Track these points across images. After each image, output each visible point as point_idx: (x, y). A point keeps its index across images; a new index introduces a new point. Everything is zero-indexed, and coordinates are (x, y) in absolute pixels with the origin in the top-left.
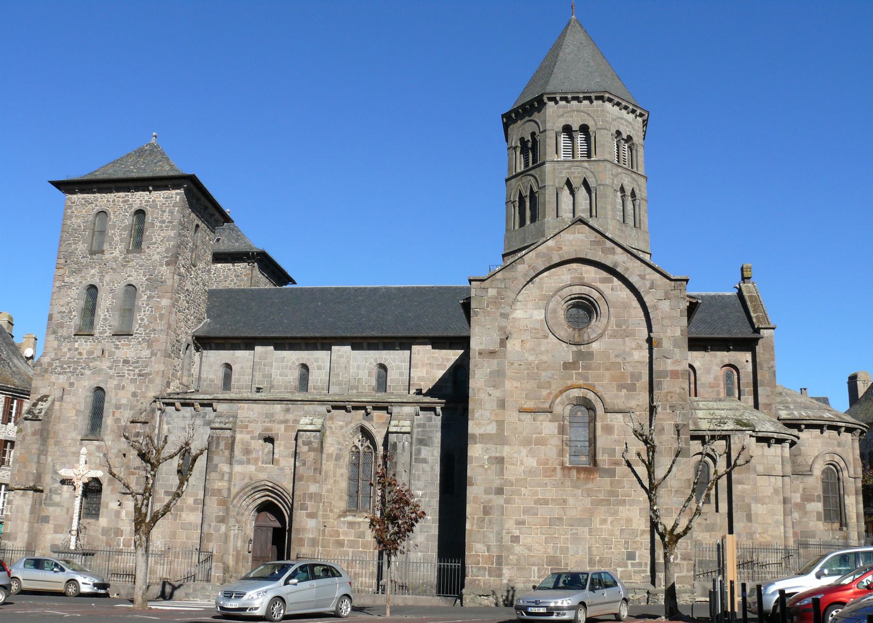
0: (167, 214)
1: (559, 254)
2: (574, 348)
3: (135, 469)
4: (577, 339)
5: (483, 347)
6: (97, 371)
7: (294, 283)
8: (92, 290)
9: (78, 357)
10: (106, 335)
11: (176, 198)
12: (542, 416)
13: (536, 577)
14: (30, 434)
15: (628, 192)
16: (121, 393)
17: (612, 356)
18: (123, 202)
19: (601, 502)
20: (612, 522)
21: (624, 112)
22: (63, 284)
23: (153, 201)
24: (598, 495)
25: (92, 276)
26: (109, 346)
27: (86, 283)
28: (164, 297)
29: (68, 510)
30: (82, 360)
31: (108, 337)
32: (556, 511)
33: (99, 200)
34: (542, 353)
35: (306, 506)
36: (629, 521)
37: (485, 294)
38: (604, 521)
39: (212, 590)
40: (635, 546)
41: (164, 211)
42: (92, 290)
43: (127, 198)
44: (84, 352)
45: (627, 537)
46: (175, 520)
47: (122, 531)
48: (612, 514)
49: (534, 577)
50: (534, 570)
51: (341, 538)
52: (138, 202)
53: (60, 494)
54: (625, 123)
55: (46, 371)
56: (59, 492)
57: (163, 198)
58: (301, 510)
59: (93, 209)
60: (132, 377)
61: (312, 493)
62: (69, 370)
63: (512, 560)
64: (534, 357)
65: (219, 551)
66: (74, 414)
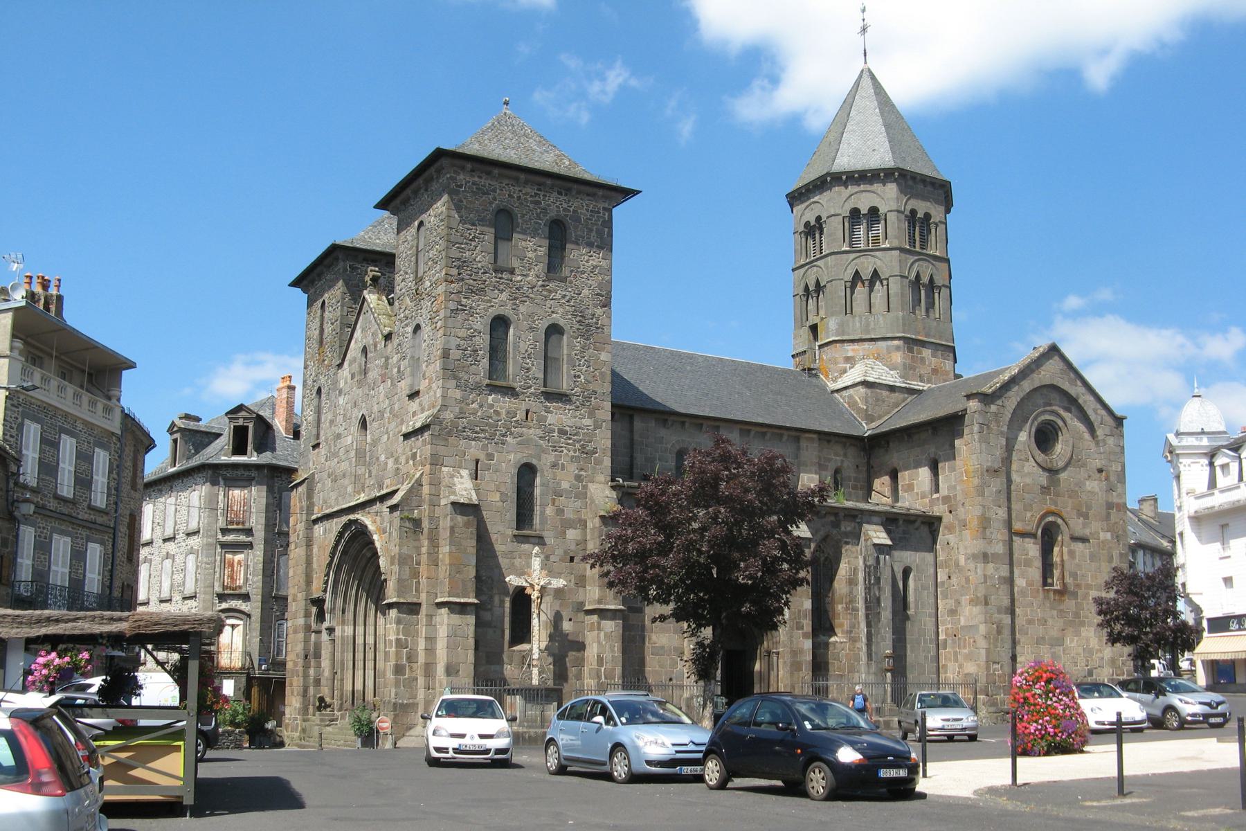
0: (594, 234)
6: (525, 443)
8: (500, 324)
9: (495, 418)
14: (461, 525)
22: (459, 307)
23: (574, 211)
25: (500, 303)
26: (536, 405)
27: (493, 312)
28: (603, 350)
30: (500, 423)
32: (1041, 631)
33: (498, 191)
36: (1088, 640)
38: (1072, 641)
39: (1056, 708)
41: (591, 230)
42: (500, 324)
43: (537, 199)
44: (503, 412)
52: (553, 207)
55: (450, 434)
56: (489, 607)
57: (587, 210)
58: (797, 629)
59: (491, 203)
60: (572, 453)
62: (482, 435)
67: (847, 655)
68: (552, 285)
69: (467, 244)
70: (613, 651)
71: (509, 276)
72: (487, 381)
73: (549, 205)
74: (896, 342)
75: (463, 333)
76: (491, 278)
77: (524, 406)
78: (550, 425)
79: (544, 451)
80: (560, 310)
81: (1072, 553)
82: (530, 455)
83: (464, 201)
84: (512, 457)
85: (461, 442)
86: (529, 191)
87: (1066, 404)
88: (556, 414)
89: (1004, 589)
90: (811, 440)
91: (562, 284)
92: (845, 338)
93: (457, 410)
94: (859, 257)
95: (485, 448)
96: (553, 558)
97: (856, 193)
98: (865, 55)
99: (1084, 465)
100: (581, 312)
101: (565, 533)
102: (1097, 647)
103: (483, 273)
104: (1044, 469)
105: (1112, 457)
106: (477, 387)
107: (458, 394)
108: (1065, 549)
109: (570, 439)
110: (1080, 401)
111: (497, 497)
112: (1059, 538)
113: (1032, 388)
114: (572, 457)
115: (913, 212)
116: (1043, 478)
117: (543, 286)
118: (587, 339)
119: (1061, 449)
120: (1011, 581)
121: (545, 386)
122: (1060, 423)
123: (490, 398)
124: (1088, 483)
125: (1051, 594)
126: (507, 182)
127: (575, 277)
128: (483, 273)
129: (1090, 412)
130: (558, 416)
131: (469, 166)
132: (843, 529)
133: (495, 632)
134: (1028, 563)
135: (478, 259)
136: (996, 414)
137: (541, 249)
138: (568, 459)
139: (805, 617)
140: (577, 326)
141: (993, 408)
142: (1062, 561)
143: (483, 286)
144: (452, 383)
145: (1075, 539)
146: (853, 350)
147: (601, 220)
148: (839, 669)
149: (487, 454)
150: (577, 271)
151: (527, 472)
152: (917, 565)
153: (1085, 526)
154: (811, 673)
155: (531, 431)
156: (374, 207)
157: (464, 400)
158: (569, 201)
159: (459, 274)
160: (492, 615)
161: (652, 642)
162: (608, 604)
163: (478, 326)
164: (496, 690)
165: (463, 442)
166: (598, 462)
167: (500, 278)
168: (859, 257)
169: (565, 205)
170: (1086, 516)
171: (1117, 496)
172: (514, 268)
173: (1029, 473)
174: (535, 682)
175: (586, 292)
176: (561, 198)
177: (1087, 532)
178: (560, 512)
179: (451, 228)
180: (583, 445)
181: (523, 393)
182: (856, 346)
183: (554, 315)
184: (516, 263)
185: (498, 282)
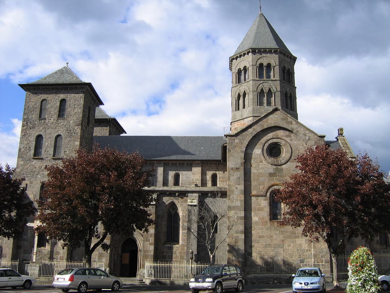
1: (267, 124)
2: (274, 167)
4: (276, 163)
5: (233, 166)
7: (126, 133)
8: (39, 138)
10: (48, 158)
12: (260, 198)
13: (259, 271)
15: (289, 95)
17: (292, 170)
19: (288, 237)
20: (293, 246)
21: (286, 57)
24: (286, 234)
27: (37, 134)
29: (30, 242)
30: (36, 171)
31: (50, 160)
32: (268, 241)
34: (259, 169)
36: (300, 245)
37: (234, 142)
38: (289, 246)
40: (304, 257)
42: (39, 138)
45: (300, 252)
47: (59, 253)
48: (293, 242)
49: (258, 271)
50: (258, 268)
51: (165, 254)
53: (26, 235)
54: (287, 63)
61: (152, 234)
62: (30, 175)
63: (248, 264)
64: (256, 171)
65: (107, 262)
77: (45, 164)
80: (61, 130)
106: (30, 160)
107: (22, 163)
115: (261, 65)
116: (271, 169)
131: (32, 88)
133: (27, 242)
134: (261, 209)
135: (34, 117)
137: (56, 110)
140: (68, 134)
144: (21, 159)
156: (104, 105)
158: (68, 92)
160: (27, 236)
172: (46, 118)
175: (71, 122)
184: (46, 117)
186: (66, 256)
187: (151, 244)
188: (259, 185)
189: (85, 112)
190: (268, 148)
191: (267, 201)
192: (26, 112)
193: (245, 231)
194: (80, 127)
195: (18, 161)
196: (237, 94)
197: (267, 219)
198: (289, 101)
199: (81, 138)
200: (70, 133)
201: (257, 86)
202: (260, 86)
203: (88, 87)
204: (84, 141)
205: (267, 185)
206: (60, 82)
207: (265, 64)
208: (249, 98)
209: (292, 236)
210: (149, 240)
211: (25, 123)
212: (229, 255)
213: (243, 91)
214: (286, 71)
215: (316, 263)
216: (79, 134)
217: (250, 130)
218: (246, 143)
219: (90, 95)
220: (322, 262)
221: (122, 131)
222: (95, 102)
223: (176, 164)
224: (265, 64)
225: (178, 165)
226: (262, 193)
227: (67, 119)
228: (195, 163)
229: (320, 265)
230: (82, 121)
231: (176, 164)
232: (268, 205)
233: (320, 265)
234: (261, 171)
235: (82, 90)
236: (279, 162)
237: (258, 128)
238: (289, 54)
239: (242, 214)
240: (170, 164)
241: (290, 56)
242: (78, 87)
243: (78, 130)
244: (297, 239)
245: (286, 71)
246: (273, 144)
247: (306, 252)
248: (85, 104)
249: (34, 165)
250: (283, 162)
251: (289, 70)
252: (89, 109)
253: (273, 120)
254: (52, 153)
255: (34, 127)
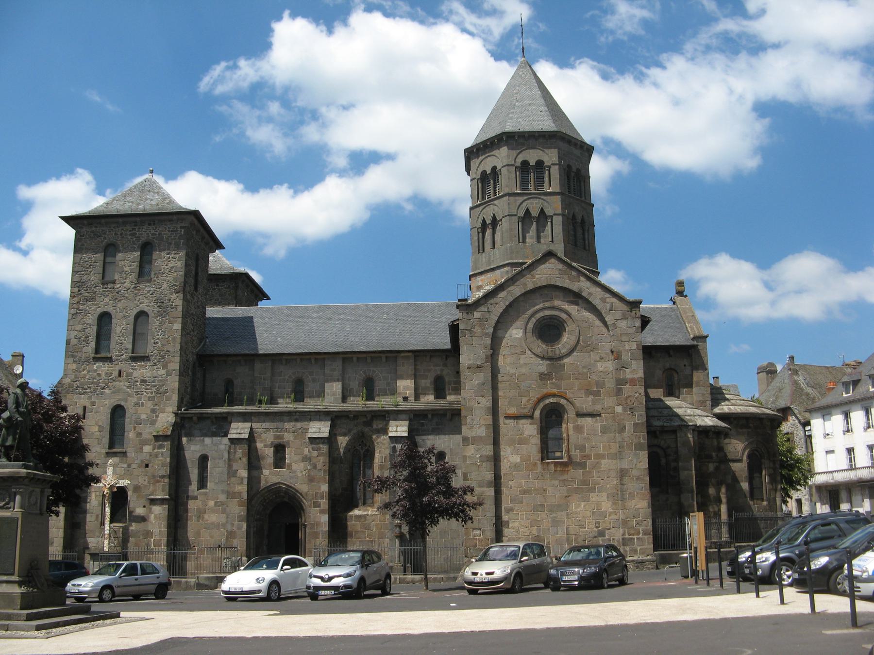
3: (160, 477)
4: (550, 354)
5: (471, 362)
6: (117, 391)
8: (105, 319)
9: (98, 378)
11: (181, 231)
16: (140, 409)
18: (130, 235)
19: (577, 491)
23: (160, 234)
24: (572, 484)
25: (104, 304)
26: (126, 367)
27: (99, 311)
32: (539, 500)
33: (107, 233)
35: (319, 503)
36: (598, 504)
38: (578, 506)
40: (604, 525)
42: (105, 319)
43: (134, 231)
44: (103, 374)
46: (198, 521)
47: (152, 533)
52: (145, 235)
57: (169, 231)
62: (89, 390)
66: (97, 430)
67: (377, 525)
68: (141, 286)
69: (85, 271)
70: (160, 527)
71: (112, 285)
72: (93, 355)
73: (142, 234)
74: (506, 269)
75: (79, 327)
76: (100, 289)
77: (117, 368)
78: (135, 378)
79: (130, 395)
81: (579, 429)
82: (120, 400)
83: (85, 244)
84: (107, 402)
85: (75, 397)
86: (128, 227)
87: (572, 299)
88: (139, 370)
89: (489, 465)
90: (407, 358)
91: (148, 284)
92: (478, 271)
93: (73, 376)
94: (485, 207)
95: (90, 398)
96: (133, 466)
97: (484, 159)
98: (523, 52)
99: (594, 349)
100: (161, 299)
101: (142, 449)
102: (610, 510)
103: (95, 287)
104: (543, 358)
105: (624, 338)
106: (87, 361)
107: (74, 366)
108: (571, 426)
109: (148, 385)
110: (584, 294)
111: (96, 429)
112: (566, 416)
113: (524, 291)
114: (149, 397)
115: (525, 163)
116: (543, 366)
117: (135, 287)
118: (164, 317)
119: (567, 340)
120: (496, 459)
121: (133, 352)
122: (564, 316)
123: (95, 366)
124: (599, 364)
125: (552, 467)
126: (113, 226)
127: (158, 277)
128: (95, 287)
129: (596, 302)
130: (142, 371)
131: (85, 222)
132: (375, 426)
134: (523, 441)
135: (91, 279)
136: (480, 320)
138: (147, 399)
139: (322, 497)
140: (158, 309)
141: (477, 315)
142: (568, 435)
143: (94, 295)
144: (71, 360)
145: (579, 415)
146: (482, 280)
147: (178, 235)
148: (370, 536)
149: (91, 402)
150: (160, 272)
151: (118, 412)
152: (451, 450)
153: (594, 402)
154: (327, 540)
155: (121, 384)
156: (224, 248)
157: (78, 370)
158: (156, 228)
159: (79, 291)
161: (204, 520)
162: (157, 495)
163: (89, 321)
164: (414, 549)
165: (76, 396)
166: (168, 399)
167: (106, 288)
168: (485, 207)
169: (153, 231)
170: (597, 394)
171: (631, 372)
172: (115, 280)
173: (525, 364)
174: (106, 549)
175: (165, 285)
176: (150, 227)
177: (598, 407)
178: (139, 434)
179: (76, 263)
180: (158, 388)
181: (117, 360)
182: (483, 277)
183: (141, 305)
184: (117, 277)
185: (104, 291)
186: (164, 540)
187: (322, 512)
188: (521, 395)
189: (189, 265)
190: (544, 318)
191: (535, 426)
192: (76, 269)
193: (495, 483)
194: (181, 295)
195: (66, 364)
196: (480, 220)
197: (537, 458)
198: (579, 231)
199: (184, 317)
200: (164, 309)
201: (518, 204)
202: (524, 204)
203: (193, 218)
204: (189, 321)
205: (535, 395)
206: (140, 208)
207: (532, 162)
208: (504, 226)
209: (582, 488)
210: (319, 503)
211: (76, 290)
212: (763, 533)
213: (492, 215)
214: (573, 174)
215: (627, 536)
216: (180, 308)
217: (502, 294)
218: (494, 318)
219: (198, 231)
220: (638, 533)
221: (260, 295)
222: (207, 244)
223: (366, 358)
224: (532, 162)
225: (369, 360)
226: (526, 411)
227: (155, 281)
228: (402, 357)
229: (634, 539)
230: (185, 282)
231: (366, 358)
232: (537, 432)
233: (634, 539)
234: (523, 370)
235: (183, 225)
236: (557, 352)
237: (517, 290)
238: (576, 145)
239: (489, 450)
240: (355, 359)
241: (581, 145)
242: (175, 217)
243: (178, 301)
244: (592, 494)
245: (573, 174)
246: (544, 319)
247: (609, 515)
248: (190, 250)
249: (96, 370)
250: (564, 351)
251: (578, 170)
252: (197, 259)
253: (549, 273)
254: (130, 346)
255: (92, 299)
